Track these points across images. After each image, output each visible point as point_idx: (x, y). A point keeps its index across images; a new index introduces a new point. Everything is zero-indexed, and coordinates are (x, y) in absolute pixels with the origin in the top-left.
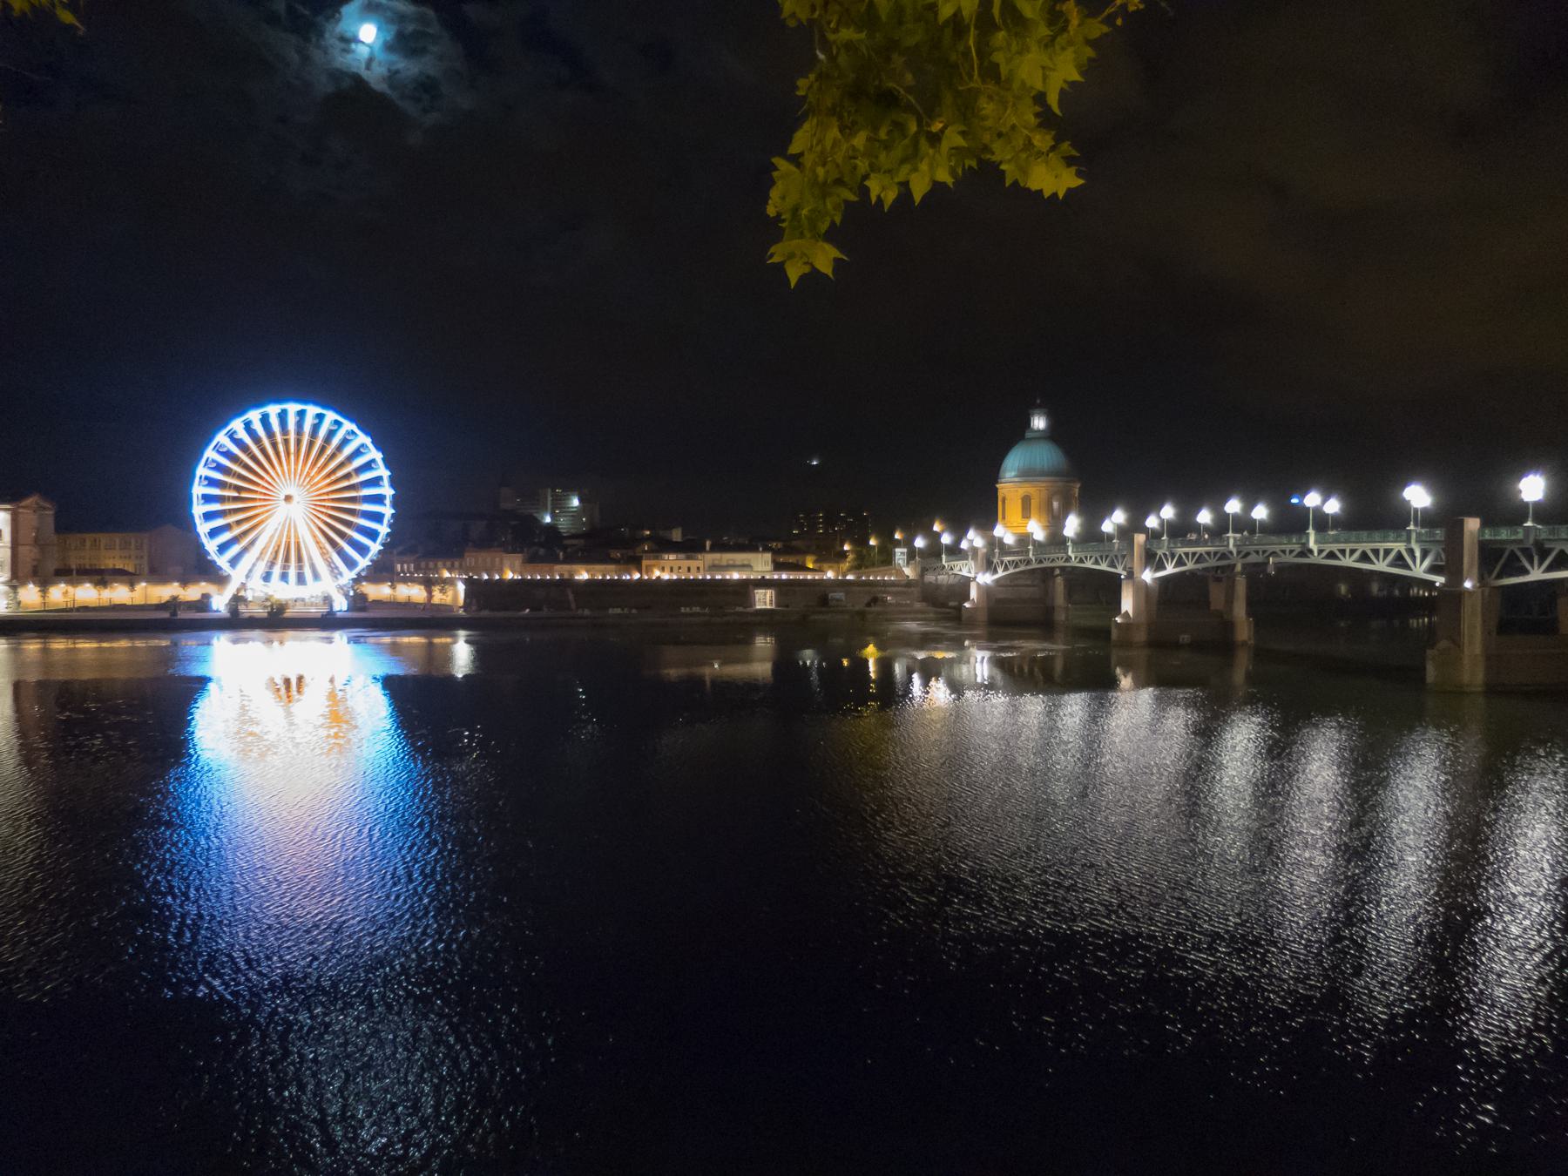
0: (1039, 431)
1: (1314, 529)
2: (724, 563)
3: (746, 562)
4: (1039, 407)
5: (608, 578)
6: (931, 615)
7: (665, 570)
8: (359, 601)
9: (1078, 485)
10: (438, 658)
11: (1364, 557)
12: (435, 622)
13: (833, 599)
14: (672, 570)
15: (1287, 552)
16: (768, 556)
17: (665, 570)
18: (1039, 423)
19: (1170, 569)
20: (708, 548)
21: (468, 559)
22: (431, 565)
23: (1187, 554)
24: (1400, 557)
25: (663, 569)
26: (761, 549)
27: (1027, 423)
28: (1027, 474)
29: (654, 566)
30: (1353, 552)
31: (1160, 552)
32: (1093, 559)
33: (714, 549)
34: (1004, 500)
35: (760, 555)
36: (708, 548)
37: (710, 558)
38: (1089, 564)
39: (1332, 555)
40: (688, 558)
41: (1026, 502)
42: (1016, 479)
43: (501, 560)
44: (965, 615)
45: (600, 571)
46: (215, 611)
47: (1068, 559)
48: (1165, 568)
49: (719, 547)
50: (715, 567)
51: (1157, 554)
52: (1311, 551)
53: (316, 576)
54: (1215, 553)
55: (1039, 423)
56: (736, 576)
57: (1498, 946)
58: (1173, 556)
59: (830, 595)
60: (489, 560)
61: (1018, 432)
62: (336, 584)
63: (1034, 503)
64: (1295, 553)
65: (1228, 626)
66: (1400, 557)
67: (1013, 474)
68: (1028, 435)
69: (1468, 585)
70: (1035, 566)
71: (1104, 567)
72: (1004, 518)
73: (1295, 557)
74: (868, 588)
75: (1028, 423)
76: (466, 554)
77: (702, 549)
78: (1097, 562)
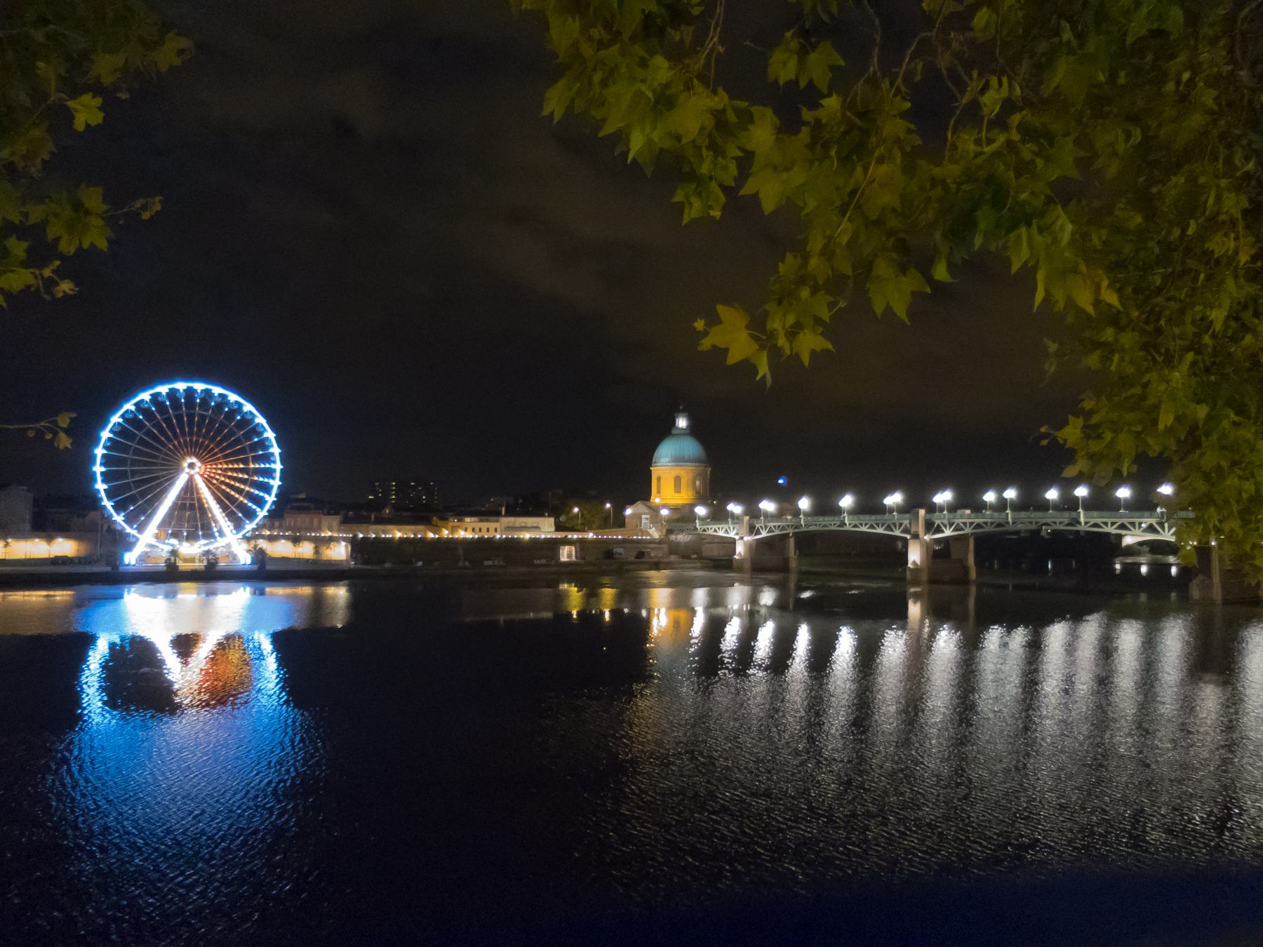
0: (682, 429)
1: (1011, 510)
2: (517, 525)
3: (535, 525)
4: (683, 411)
5: (419, 536)
6: (699, 565)
7: (466, 531)
8: (260, 556)
9: (710, 469)
10: (318, 605)
11: (715, 531)
12: (320, 574)
13: (616, 553)
14: (473, 530)
15: (1109, 525)
16: (552, 520)
17: (466, 531)
18: (682, 423)
19: (764, 534)
20: (503, 513)
21: (288, 520)
22: (316, 521)
23: (775, 526)
24: (726, 530)
25: (466, 530)
26: (36, 510)
27: (673, 423)
28: (679, 460)
29: (459, 527)
30: (866, 525)
31: (758, 526)
32: (724, 530)
33: (509, 514)
34: (659, 479)
35: (547, 519)
36: (503, 513)
37: (506, 521)
38: (864, 529)
39: (1096, 525)
40: (481, 521)
41: (677, 480)
42: (670, 464)
43: (320, 522)
44: (735, 564)
45: (411, 530)
46: (128, 565)
47: (843, 524)
48: (761, 534)
49: (511, 512)
50: (510, 528)
51: (934, 523)
52: (845, 524)
53: (221, 533)
54: (779, 526)
55: (682, 423)
56: (527, 536)
57: (1038, 755)
58: (766, 527)
59: (615, 550)
60: (307, 520)
61: (667, 429)
62: (240, 535)
63: (683, 482)
64: (1089, 524)
65: (966, 570)
66: (726, 530)
67: (667, 460)
68: (674, 432)
69: (1213, 543)
70: (804, 529)
71: (880, 530)
72: (659, 492)
73: (1116, 529)
74: (635, 545)
75: (673, 423)
76: (286, 516)
77: (498, 514)
78: (872, 527)
